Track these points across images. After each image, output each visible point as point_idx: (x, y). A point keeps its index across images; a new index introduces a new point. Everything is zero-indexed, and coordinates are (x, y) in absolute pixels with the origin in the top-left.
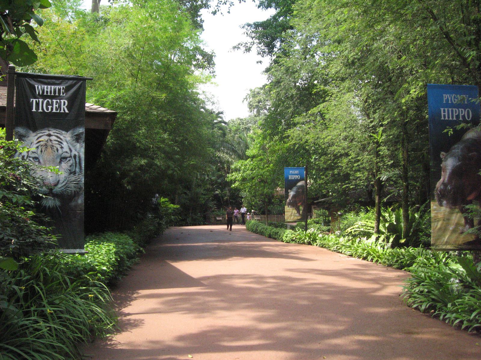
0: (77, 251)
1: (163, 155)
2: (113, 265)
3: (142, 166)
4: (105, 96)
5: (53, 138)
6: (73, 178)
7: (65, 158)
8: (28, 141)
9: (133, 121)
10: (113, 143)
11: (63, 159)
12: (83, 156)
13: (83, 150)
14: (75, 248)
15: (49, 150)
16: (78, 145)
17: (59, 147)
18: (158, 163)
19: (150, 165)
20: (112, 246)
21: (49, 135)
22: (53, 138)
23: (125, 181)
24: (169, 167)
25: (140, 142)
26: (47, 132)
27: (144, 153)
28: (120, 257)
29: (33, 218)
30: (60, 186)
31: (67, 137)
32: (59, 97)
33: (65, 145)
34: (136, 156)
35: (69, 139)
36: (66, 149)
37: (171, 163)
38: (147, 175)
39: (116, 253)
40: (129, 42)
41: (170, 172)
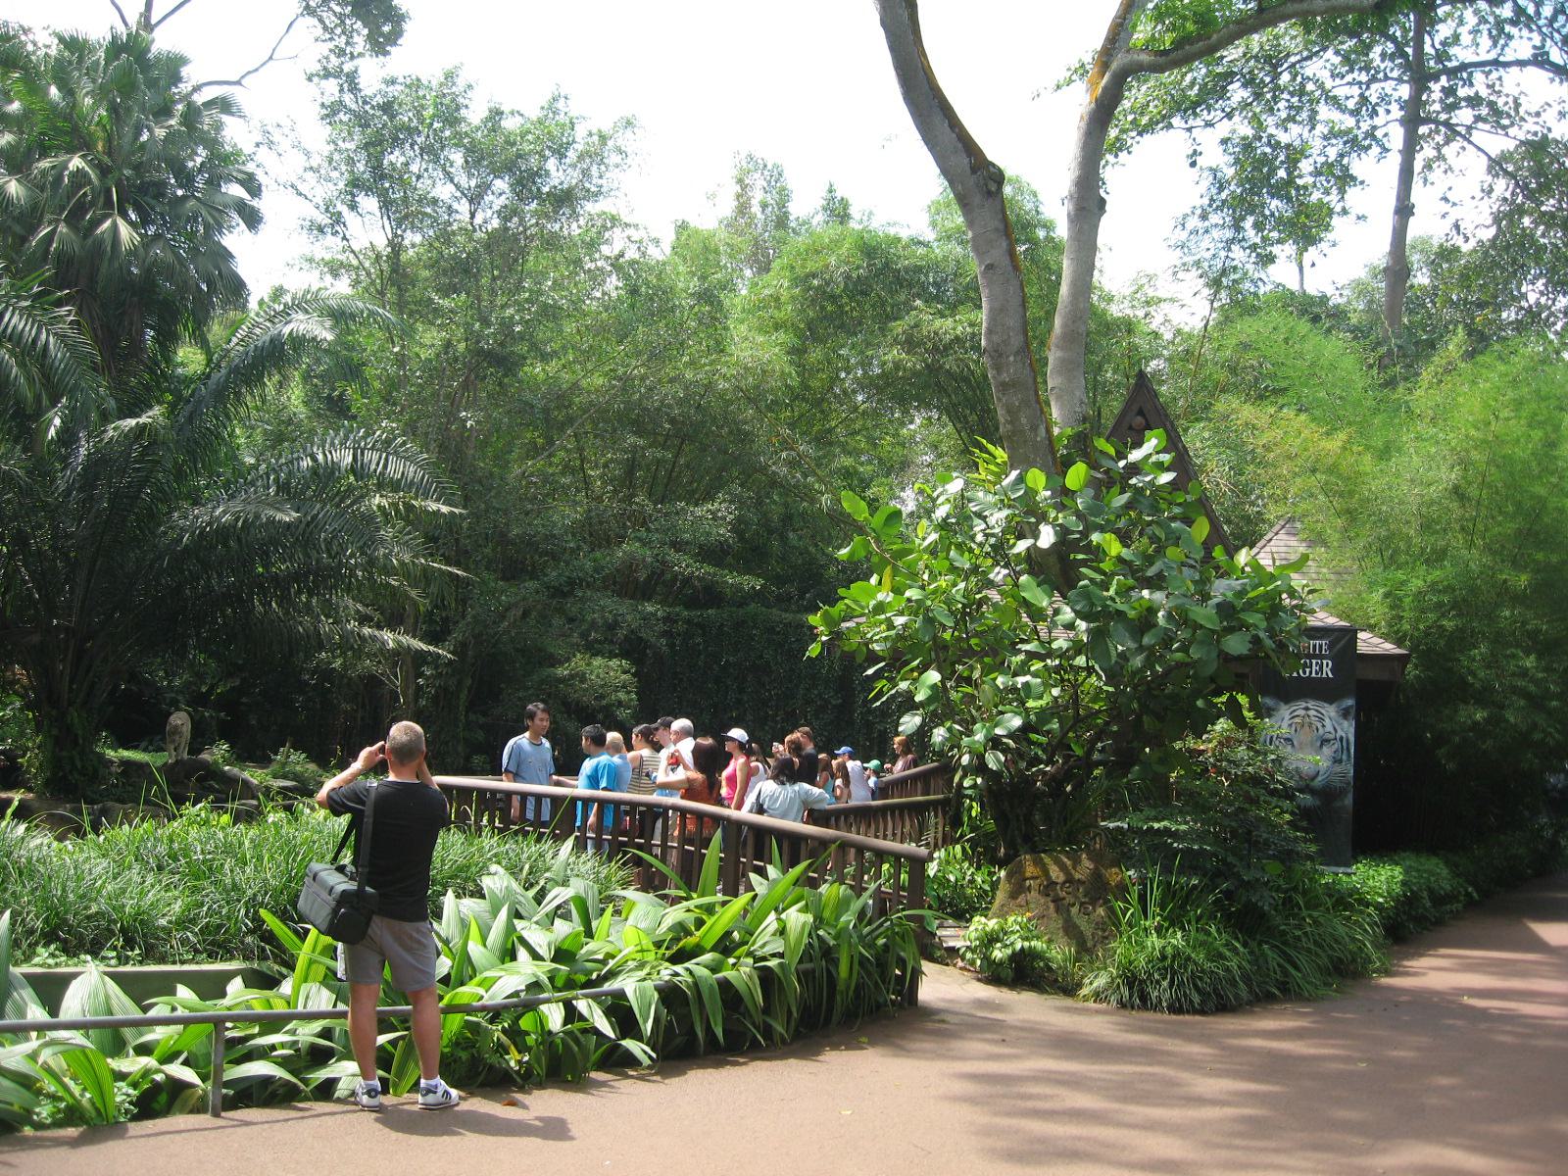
0: (1341, 870)
1: (1522, 703)
2: (1396, 899)
3: (1476, 723)
4: (1403, 583)
5: (1312, 713)
6: (1338, 768)
7: (1328, 741)
8: (1278, 715)
9: (1460, 630)
10: (1417, 677)
11: (1324, 741)
12: (1352, 739)
13: (1352, 730)
14: (1338, 865)
15: (1306, 728)
16: (1346, 724)
17: (1319, 725)
18: (1512, 720)
19: (1495, 720)
20: (1398, 870)
21: (1307, 709)
22: (1312, 713)
23: (1442, 752)
24: (1535, 725)
25: (1473, 674)
26: (1304, 705)
27: (1483, 697)
28: (1412, 891)
29: (1288, 823)
30: (1320, 778)
31: (1330, 711)
32: (1321, 657)
33: (1327, 722)
34: (1466, 703)
35: (1333, 714)
36: (1329, 728)
37: (1540, 719)
38: (1490, 743)
39: (1404, 883)
40: (1450, 476)
41: (1537, 736)
